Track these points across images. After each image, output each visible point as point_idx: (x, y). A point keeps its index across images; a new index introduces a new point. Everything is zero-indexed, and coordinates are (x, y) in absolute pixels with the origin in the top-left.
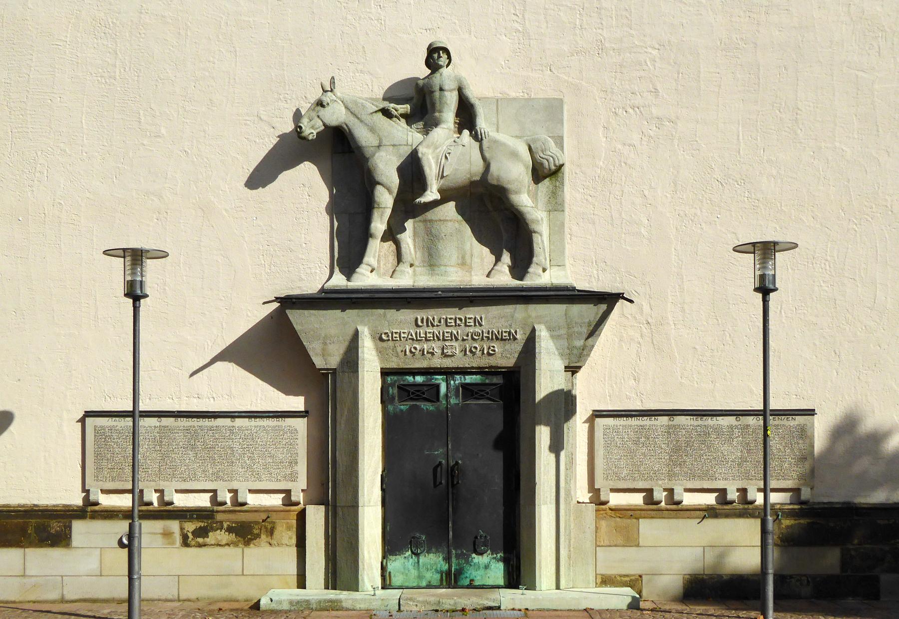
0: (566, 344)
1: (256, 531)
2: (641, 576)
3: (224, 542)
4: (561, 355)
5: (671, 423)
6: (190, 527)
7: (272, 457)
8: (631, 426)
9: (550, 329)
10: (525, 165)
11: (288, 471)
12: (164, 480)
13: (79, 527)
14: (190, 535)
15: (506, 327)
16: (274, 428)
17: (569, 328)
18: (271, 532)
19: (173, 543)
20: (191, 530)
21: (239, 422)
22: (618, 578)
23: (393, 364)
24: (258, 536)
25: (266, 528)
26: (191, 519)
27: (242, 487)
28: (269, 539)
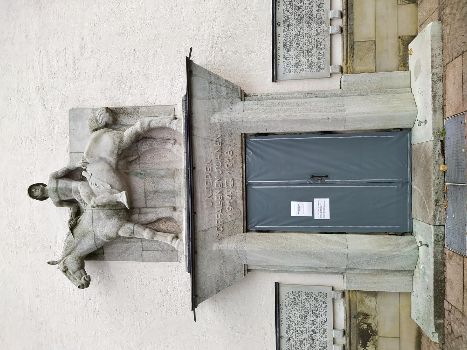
0: (224, 100)
1: (366, 327)
2: (399, 37)
4: (233, 104)
5: (282, 24)
8: (284, 53)
9: (214, 112)
10: (105, 133)
11: (319, 299)
15: (213, 143)
16: (288, 308)
17: (213, 98)
18: (366, 315)
21: (284, 333)
22: (401, 54)
23: (240, 224)
24: (369, 325)
25: (363, 319)
28: (372, 317)
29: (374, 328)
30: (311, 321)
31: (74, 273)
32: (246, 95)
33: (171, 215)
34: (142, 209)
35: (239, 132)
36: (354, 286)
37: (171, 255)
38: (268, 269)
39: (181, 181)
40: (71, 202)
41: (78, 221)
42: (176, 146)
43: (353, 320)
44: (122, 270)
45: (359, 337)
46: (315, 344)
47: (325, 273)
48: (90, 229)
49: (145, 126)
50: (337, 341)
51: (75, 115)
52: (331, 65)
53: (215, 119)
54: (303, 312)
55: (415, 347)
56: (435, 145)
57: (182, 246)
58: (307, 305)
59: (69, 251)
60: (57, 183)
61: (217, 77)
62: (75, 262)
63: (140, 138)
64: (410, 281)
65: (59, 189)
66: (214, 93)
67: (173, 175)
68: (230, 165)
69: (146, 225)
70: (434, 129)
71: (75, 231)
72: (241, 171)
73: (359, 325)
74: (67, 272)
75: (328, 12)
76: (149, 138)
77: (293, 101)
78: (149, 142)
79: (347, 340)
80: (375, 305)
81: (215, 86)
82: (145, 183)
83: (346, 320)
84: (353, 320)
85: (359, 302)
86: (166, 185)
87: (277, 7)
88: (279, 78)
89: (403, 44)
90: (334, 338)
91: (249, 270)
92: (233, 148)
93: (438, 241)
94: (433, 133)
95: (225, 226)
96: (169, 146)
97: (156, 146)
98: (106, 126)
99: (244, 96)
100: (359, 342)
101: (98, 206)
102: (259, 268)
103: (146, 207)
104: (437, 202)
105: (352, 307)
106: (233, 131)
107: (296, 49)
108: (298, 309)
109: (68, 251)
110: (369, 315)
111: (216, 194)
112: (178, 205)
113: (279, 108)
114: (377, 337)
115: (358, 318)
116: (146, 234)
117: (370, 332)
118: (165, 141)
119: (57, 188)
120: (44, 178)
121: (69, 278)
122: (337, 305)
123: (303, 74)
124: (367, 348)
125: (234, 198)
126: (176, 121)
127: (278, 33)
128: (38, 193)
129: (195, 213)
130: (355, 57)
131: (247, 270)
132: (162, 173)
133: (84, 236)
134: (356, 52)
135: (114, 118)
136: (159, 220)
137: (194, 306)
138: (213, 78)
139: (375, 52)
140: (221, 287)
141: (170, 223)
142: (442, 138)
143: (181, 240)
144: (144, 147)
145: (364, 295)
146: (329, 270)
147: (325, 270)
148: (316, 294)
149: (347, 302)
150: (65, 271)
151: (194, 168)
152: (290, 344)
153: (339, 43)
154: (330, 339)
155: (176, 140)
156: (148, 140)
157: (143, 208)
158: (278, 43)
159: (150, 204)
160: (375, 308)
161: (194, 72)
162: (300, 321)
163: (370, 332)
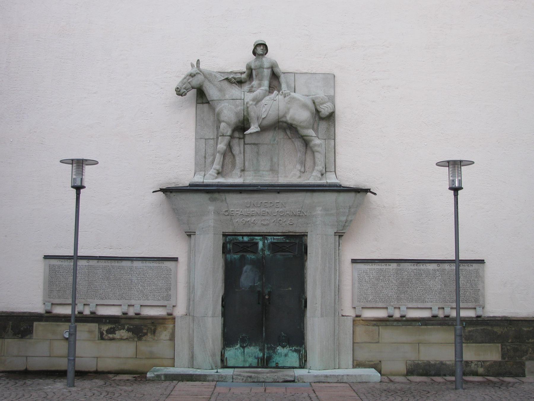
1: (145, 331)
2: (380, 361)
3: (125, 337)
5: (398, 267)
8: (374, 269)
12: (90, 299)
14: (105, 332)
15: (299, 209)
17: (337, 209)
18: (154, 332)
21: (136, 264)
22: (367, 362)
24: (146, 334)
25: (151, 329)
26: (105, 323)
27: (137, 303)
31: (189, 83)
32: (340, 236)
33: (237, 167)
34: (242, 140)
35: (309, 230)
36: (178, 322)
37: (201, 164)
38: (191, 252)
39: (267, 179)
40: (250, 76)
41: (234, 84)
42: (298, 173)
44: (187, 115)
47: (189, 300)
48: (227, 97)
49: (316, 148)
50: (87, 307)
51: (330, 79)
52: (362, 308)
53: (319, 211)
56: (291, 376)
57: (210, 178)
59: (207, 76)
60: (268, 68)
61: (355, 213)
62: (199, 83)
63: (306, 142)
65: (262, 70)
66: (341, 210)
67: (273, 170)
68: (281, 222)
69: (229, 146)
70: (303, 376)
71: (226, 82)
72: (275, 231)
74: (190, 77)
75: (404, 305)
76: (306, 148)
77: (333, 276)
78: (303, 149)
81: (347, 211)
82: (266, 144)
86: (264, 163)
87: (413, 264)
88: (354, 265)
89: (375, 364)
90: (133, 305)
91: (189, 236)
92: (295, 225)
93: (222, 378)
94: (300, 375)
95: (229, 217)
96: (298, 167)
97: (299, 154)
98: (318, 111)
99: (340, 235)
101: (248, 107)
102: (192, 245)
103: (245, 144)
104: (250, 377)
105: (161, 321)
106: (310, 225)
107: (378, 279)
109: (208, 76)
111: (256, 209)
112: (246, 173)
113: (327, 265)
114: (136, 340)
116: (222, 146)
118: (303, 163)
119: (263, 68)
120: (272, 55)
121: (185, 78)
122: (161, 309)
123: (357, 285)
125: (252, 225)
126: (320, 176)
127: (392, 264)
128: (260, 50)
129: (241, 193)
130: (367, 326)
131: (189, 235)
132: (275, 160)
133: (221, 90)
134: (371, 328)
135: (326, 118)
136: (234, 156)
137: (161, 190)
138: (354, 211)
139: (370, 343)
140: (176, 213)
141: (230, 166)
142: (296, 381)
143: (216, 178)
144: (298, 144)
146: (191, 303)
147: (191, 299)
150: (192, 75)
151: (279, 193)
153: (382, 314)
154: (133, 302)
155: (304, 173)
156: (305, 148)
157: (244, 142)
158: (383, 264)
159: (248, 147)
161: (359, 195)
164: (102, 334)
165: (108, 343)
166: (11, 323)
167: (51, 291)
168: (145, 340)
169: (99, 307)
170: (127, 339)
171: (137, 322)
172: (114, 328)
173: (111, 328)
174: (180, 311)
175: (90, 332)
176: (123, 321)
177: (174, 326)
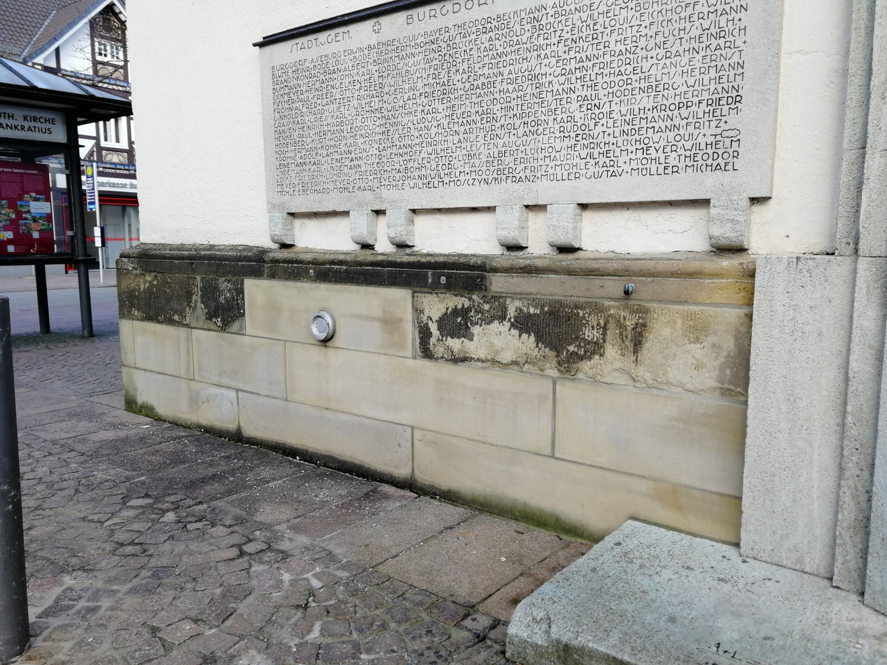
1: (590, 334)
3: (507, 357)
6: (436, 306)
7: (653, 88)
12: (390, 187)
13: (256, 291)
14: (434, 328)
18: (637, 340)
19: (402, 347)
20: (436, 317)
24: (596, 349)
25: (621, 326)
26: (435, 288)
27: (560, 193)
28: (627, 362)
29: (585, 365)
30: (606, 109)
43: (614, 287)
45: (552, 303)
46: (521, 131)
50: (536, 221)
54: (646, 65)
55: (525, 504)
58: (679, 80)
64: (800, 561)
73: (597, 308)
79: (540, 257)
80: (681, 385)
83: (617, 257)
84: (614, 287)
85: (691, 316)
100: (535, 302)
105: (673, 285)
108: (660, 39)
110: (635, 352)
114: (553, 373)
115: (626, 307)
117: (572, 348)
124: (515, 332)
145: (729, 344)
148: (733, 120)
149: (695, 265)
152: (517, 27)
160: (668, 383)
162: (608, 58)
163: (572, 348)
164: (424, 334)
165: (446, 370)
166: (199, 278)
167: (283, 166)
168: (594, 380)
169: (421, 221)
170: (515, 363)
171: (552, 288)
172: (464, 312)
173: (456, 312)
174: (783, 233)
175: (390, 323)
176: (497, 283)
177: (750, 317)
